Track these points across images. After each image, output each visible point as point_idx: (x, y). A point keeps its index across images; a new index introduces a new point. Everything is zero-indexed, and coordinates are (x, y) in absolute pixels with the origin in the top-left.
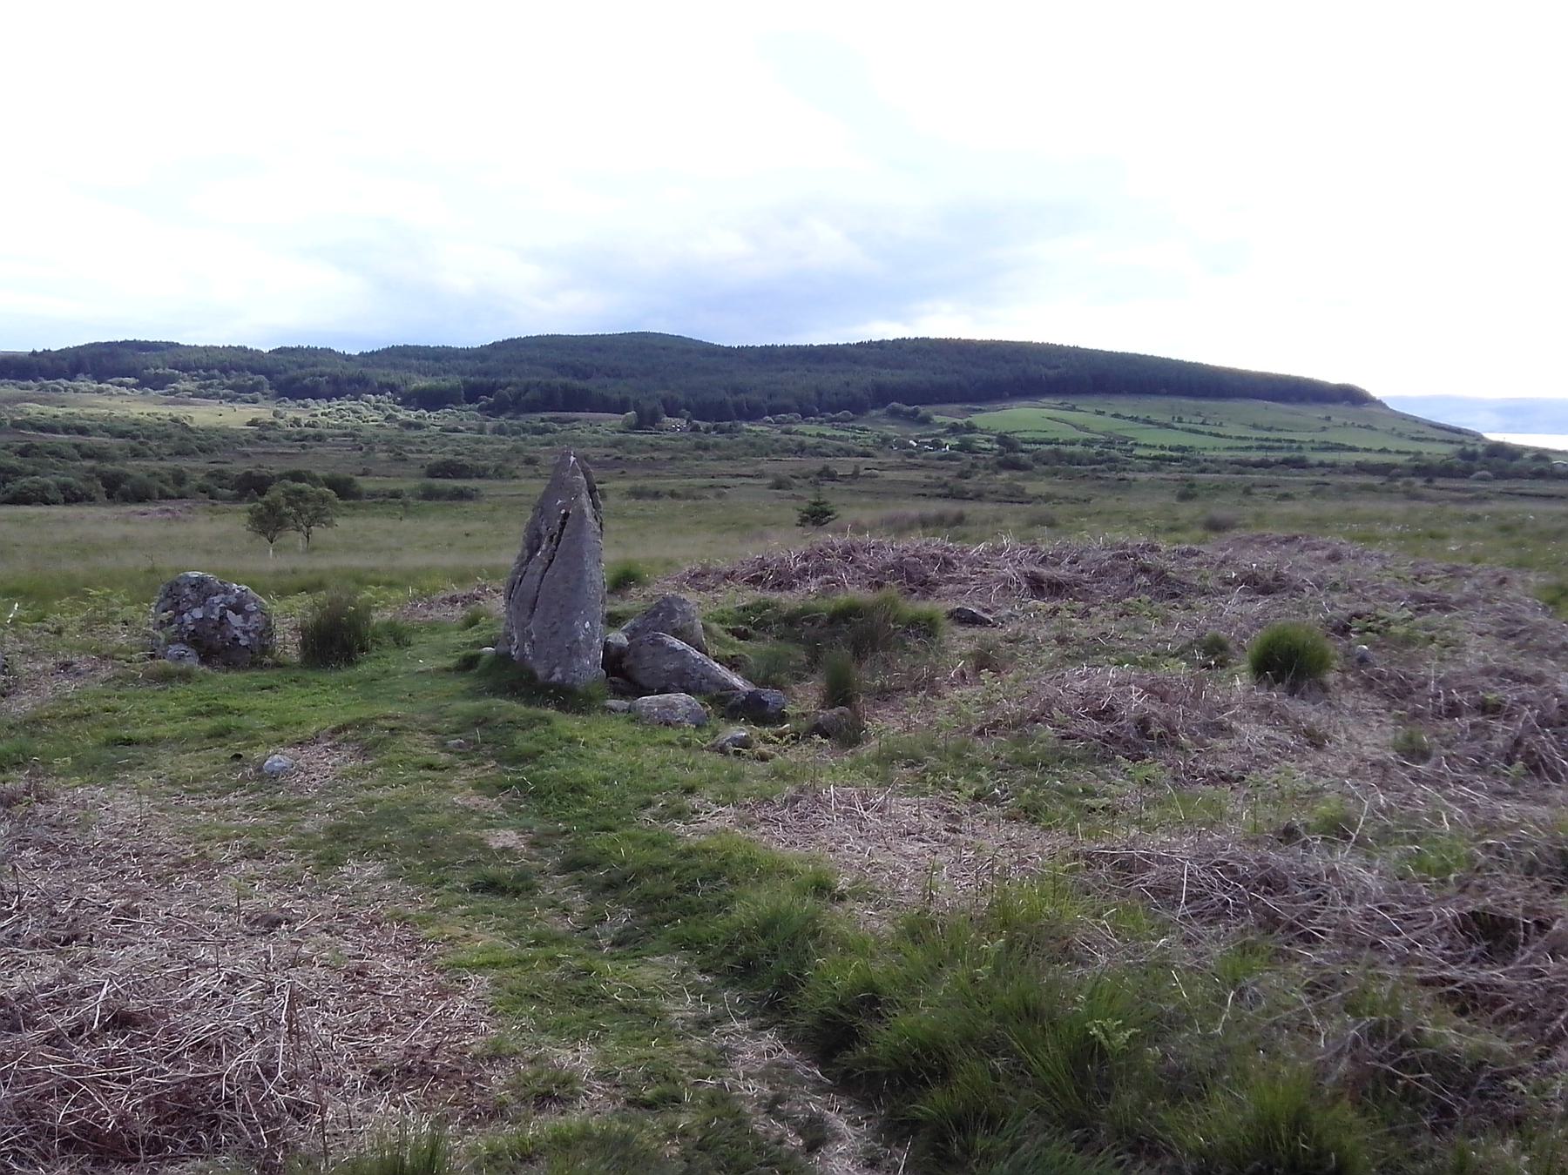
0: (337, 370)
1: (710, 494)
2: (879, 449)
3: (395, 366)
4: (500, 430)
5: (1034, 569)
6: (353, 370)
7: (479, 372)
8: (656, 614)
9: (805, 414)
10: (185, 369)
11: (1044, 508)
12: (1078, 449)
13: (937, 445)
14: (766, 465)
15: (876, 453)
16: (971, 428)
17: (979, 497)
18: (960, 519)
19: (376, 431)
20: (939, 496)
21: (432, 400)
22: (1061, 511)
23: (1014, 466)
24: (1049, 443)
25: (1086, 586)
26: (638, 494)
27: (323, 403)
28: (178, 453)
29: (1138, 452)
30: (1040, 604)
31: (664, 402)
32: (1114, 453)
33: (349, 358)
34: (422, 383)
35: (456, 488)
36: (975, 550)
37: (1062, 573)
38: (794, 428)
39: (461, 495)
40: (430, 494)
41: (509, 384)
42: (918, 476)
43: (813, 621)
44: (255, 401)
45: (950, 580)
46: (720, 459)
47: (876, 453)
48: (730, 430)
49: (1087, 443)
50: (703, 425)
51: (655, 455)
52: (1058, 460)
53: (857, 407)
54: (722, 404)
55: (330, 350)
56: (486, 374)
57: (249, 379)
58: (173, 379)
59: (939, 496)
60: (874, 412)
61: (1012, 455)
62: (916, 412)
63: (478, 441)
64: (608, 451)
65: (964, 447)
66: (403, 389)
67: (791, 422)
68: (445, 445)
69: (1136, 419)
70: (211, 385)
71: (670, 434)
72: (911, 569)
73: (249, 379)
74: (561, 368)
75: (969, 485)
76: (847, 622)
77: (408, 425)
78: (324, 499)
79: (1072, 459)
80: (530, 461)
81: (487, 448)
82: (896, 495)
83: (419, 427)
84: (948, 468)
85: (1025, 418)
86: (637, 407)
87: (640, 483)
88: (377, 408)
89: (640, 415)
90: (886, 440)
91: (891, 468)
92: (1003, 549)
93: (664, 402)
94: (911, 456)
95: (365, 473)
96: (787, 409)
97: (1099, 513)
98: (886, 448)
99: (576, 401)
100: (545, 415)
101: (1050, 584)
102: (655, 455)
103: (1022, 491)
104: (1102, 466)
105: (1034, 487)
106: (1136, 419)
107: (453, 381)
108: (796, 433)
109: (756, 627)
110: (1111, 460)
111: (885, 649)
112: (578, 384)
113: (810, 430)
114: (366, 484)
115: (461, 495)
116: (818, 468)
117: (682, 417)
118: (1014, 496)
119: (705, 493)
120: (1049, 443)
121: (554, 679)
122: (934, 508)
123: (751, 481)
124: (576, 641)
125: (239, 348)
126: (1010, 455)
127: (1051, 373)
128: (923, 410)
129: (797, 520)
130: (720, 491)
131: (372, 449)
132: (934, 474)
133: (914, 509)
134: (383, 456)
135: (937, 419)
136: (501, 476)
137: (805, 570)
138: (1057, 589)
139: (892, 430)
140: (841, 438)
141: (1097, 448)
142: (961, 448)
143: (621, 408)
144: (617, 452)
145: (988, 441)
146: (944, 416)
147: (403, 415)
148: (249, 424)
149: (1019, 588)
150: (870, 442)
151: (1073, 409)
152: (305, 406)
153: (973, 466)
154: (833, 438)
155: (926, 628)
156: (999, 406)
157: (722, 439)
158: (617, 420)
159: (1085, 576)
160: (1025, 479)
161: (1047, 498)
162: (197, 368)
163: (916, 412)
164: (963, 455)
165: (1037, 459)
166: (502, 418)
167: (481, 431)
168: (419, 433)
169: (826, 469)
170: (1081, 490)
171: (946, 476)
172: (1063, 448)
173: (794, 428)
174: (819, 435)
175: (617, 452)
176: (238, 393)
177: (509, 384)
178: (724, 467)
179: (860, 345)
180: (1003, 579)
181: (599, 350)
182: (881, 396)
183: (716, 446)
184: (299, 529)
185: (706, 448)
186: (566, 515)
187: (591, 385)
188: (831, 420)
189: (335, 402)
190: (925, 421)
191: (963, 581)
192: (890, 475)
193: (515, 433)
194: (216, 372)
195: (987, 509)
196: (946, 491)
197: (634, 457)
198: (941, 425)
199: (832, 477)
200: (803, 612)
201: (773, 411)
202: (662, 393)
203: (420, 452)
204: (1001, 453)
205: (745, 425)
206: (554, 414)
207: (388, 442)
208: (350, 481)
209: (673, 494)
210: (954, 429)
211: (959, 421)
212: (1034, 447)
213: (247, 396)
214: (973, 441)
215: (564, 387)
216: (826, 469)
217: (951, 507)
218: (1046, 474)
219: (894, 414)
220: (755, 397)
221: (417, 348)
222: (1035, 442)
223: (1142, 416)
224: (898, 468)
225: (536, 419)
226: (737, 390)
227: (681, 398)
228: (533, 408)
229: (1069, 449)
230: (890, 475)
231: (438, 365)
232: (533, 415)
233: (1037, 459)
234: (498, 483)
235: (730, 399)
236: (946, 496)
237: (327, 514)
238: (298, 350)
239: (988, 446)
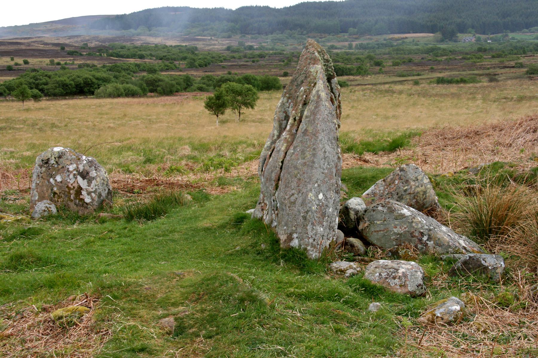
208: (275, 80)
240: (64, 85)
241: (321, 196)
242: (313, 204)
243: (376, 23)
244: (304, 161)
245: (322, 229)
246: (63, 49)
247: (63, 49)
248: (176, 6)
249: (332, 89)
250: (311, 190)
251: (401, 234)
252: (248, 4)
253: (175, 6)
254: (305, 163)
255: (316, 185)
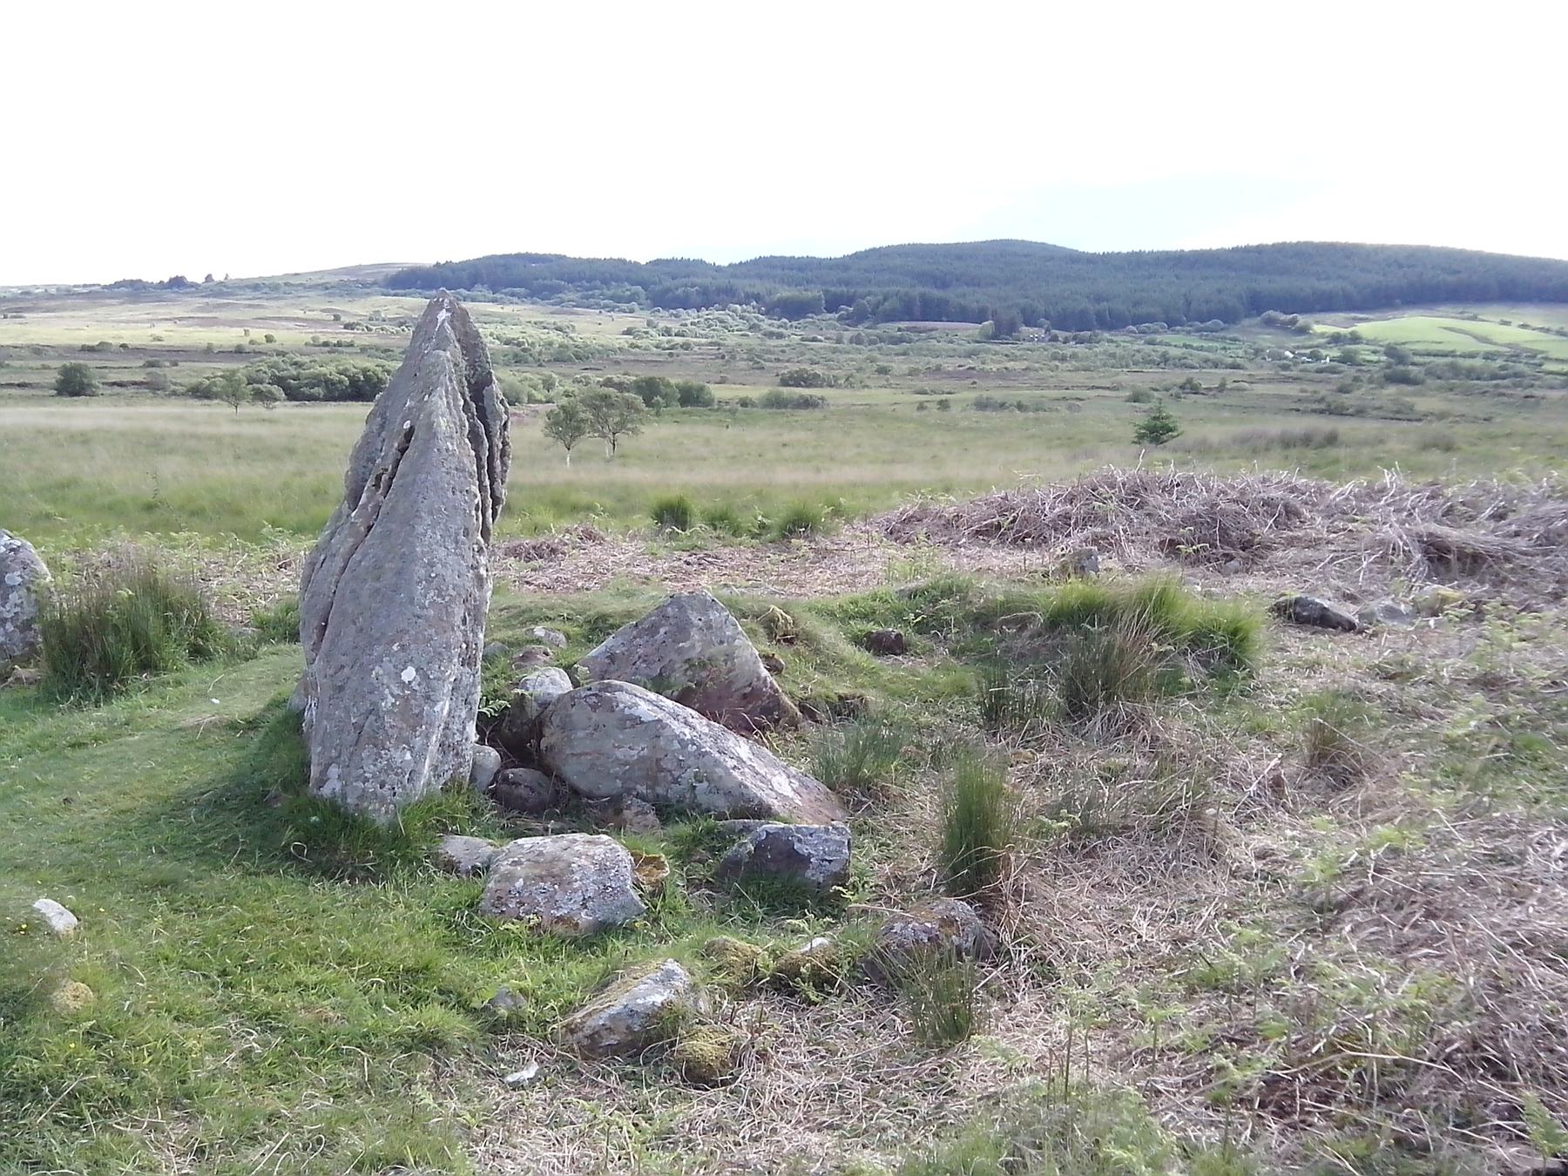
0: (707, 281)
1: (1062, 407)
2: (1251, 360)
3: (761, 277)
4: (857, 340)
5: (1434, 528)
6: (722, 282)
7: (840, 282)
8: (653, 629)
9: (1172, 323)
10: (571, 281)
11: (1437, 427)
12: (1478, 362)
13: (1316, 357)
14: (1124, 377)
15: (1247, 365)
16: (1355, 339)
17: (1360, 413)
18: (1332, 440)
19: (740, 340)
20: (1314, 411)
21: (794, 310)
22: (1461, 431)
23: (1404, 380)
24: (1445, 355)
25: (1523, 560)
26: (982, 405)
27: (693, 312)
28: (556, 360)
29: (1549, 367)
30: (1445, 590)
31: (1023, 311)
32: (1521, 367)
33: (719, 269)
34: (785, 292)
35: (801, 397)
36: (1343, 490)
37: (1476, 536)
38: (1159, 338)
39: (807, 403)
40: (775, 403)
41: (869, 294)
42: (1292, 390)
43: (1022, 624)
44: (632, 311)
45: (1291, 542)
46: (1077, 370)
47: (1247, 365)
48: (1090, 341)
49: (1488, 356)
50: (1061, 334)
51: (1010, 365)
52: (1454, 373)
53: (1230, 317)
54: (1083, 313)
55: (702, 262)
56: (847, 284)
57: (627, 289)
58: (559, 290)
59: (1314, 411)
60: (1246, 322)
61: (1401, 368)
62: (1294, 322)
63: (835, 351)
64: (962, 361)
65: (1347, 359)
66: (767, 299)
67: (1155, 332)
68: (802, 354)
69: (1548, 331)
70: (592, 296)
71: (1027, 345)
72: (1228, 523)
73: (627, 289)
74: (921, 277)
75: (1347, 399)
76: (1077, 627)
77: (770, 335)
78: (630, 405)
79: (1471, 374)
80: (883, 371)
81: (842, 357)
82: (1262, 410)
83: (780, 336)
84: (1328, 382)
85: (1418, 328)
86: (994, 315)
87: (985, 394)
88: (742, 318)
89: (998, 325)
90: (1257, 352)
91: (1262, 381)
92: (1383, 490)
93: (1023, 311)
94: (1286, 368)
95: (722, 381)
96: (1151, 319)
97: (1508, 435)
98: (1258, 360)
99: (933, 311)
100: (903, 325)
101: (1461, 555)
102: (1010, 365)
103: (1411, 408)
104: (1510, 379)
105: (1423, 404)
106: (1548, 331)
107: (814, 292)
108: (1160, 343)
109: (921, 628)
110: (1516, 375)
111: (1133, 697)
112: (937, 293)
113: (1174, 342)
114: (718, 392)
115: (807, 403)
116: (1182, 380)
117: (1040, 326)
118: (1401, 414)
119: (1056, 405)
120: (1445, 355)
121: (326, 791)
122: (1299, 425)
123: (1107, 393)
124: (373, 711)
125: (619, 260)
126: (1399, 367)
127: (1451, 279)
128: (1302, 319)
129: (1131, 434)
130: (1074, 404)
131: (733, 357)
132: (1310, 388)
133: (1276, 426)
134: (742, 364)
135: (1318, 329)
136: (851, 386)
137: (1066, 517)
138: (1474, 563)
139: (1267, 340)
140: (1209, 350)
141: (1500, 362)
142: (1343, 360)
143: (979, 317)
144: (971, 363)
145: (1374, 352)
146: (1323, 326)
147: (766, 324)
148: (625, 333)
149: (1408, 560)
150: (1241, 352)
151: (1474, 318)
152: (676, 316)
153: (1356, 379)
154: (1201, 349)
155: (1225, 651)
156: (1389, 314)
157: (1081, 349)
158: (973, 329)
159: (1522, 543)
160: (1414, 394)
161: (1441, 416)
162: (581, 279)
163: (1294, 322)
164: (1344, 367)
165: (1429, 373)
166: (860, 327)
167: (839, 341)
168: (780, 342)
169: (1189, 381)
170: (1480, 407)
171: (1323, 390)
172: (1460, 361)
173: (1159, 338)
174: (1186, 346)
175: (971, 363)
176: (618, 302)
177: (869, 294)
178: (1080, 378)
179: (1236, 250)
180: (1382, 543)
181: (959, 258)
182: (1256, 304)
183: (1074, 356)
184: (604, 436)
185: (1063, 359)
186: (409, 434)
187: (952, 295)
188: (1198, 330)
189: (704, 312)
190: (1303, 331)
191: (1314, 544)
192: (1260, 388)
193: (872, 342)
194: (598, 283)
195: (1369, 427)
196: (1323, 406)
197: (987, 367)
198: (1322, 335)
199: (1195, 390)
200: (1007, 607)
201: (1137, 321)
202: (1022, 301)
203: (778, 360)
204: (1389, 366)
205: (1106, 335)
206: (914, 324)
207: (750, 351)
208: (702, 389)
209: (1020, 407)
210: (1336, 339)
211: (1343, 331)
212: (1427, 359)
213: (624, 306)
214: (1356, 352)
215: (922, 296)
216: (1189, 381)
217: (1324, 424)
218: (1440, 389)
219: (1270, 323)
220: (1119, 306)
221: (783, 258)
222: (1428, 354)
223: (1555, 327)
224: (1270, 381)
225: (893, 328)
226: (1099, 299)
227: (1041, 308)
228: (891, 317)
229: (1467, 363)
230: (1260, 388)
231: (801, 275)
232: (890, 324)
233: (1429, 373)
234: (848, 392)
235: (1092, 308)
236: (1322, 412)
237: (632, 421)
238: (673, 261)
239: (1374, 358)
240: (328, 383)
241: (409, 674)
242: (382, 693)
243: (885, 299)
244: (378, 585)
245: (408, 756)
246: (337, 318)
247: (337, 318)
248: (541, 252)
249: (482, 414)
250: (380, 661)
251: (632, 765)
252: (666, 255)
253: (585, 257)
254: (377, 591)
255: (395, 648)
